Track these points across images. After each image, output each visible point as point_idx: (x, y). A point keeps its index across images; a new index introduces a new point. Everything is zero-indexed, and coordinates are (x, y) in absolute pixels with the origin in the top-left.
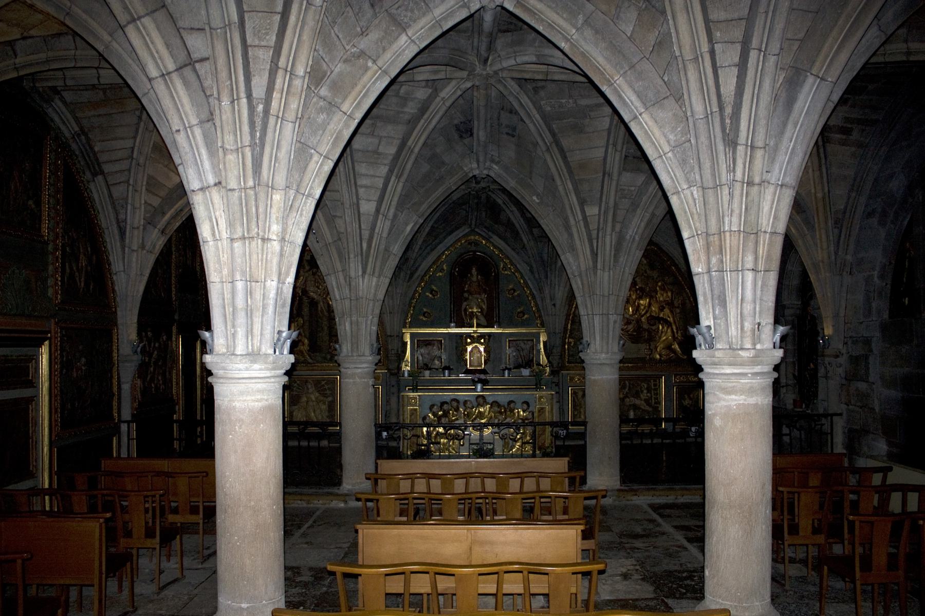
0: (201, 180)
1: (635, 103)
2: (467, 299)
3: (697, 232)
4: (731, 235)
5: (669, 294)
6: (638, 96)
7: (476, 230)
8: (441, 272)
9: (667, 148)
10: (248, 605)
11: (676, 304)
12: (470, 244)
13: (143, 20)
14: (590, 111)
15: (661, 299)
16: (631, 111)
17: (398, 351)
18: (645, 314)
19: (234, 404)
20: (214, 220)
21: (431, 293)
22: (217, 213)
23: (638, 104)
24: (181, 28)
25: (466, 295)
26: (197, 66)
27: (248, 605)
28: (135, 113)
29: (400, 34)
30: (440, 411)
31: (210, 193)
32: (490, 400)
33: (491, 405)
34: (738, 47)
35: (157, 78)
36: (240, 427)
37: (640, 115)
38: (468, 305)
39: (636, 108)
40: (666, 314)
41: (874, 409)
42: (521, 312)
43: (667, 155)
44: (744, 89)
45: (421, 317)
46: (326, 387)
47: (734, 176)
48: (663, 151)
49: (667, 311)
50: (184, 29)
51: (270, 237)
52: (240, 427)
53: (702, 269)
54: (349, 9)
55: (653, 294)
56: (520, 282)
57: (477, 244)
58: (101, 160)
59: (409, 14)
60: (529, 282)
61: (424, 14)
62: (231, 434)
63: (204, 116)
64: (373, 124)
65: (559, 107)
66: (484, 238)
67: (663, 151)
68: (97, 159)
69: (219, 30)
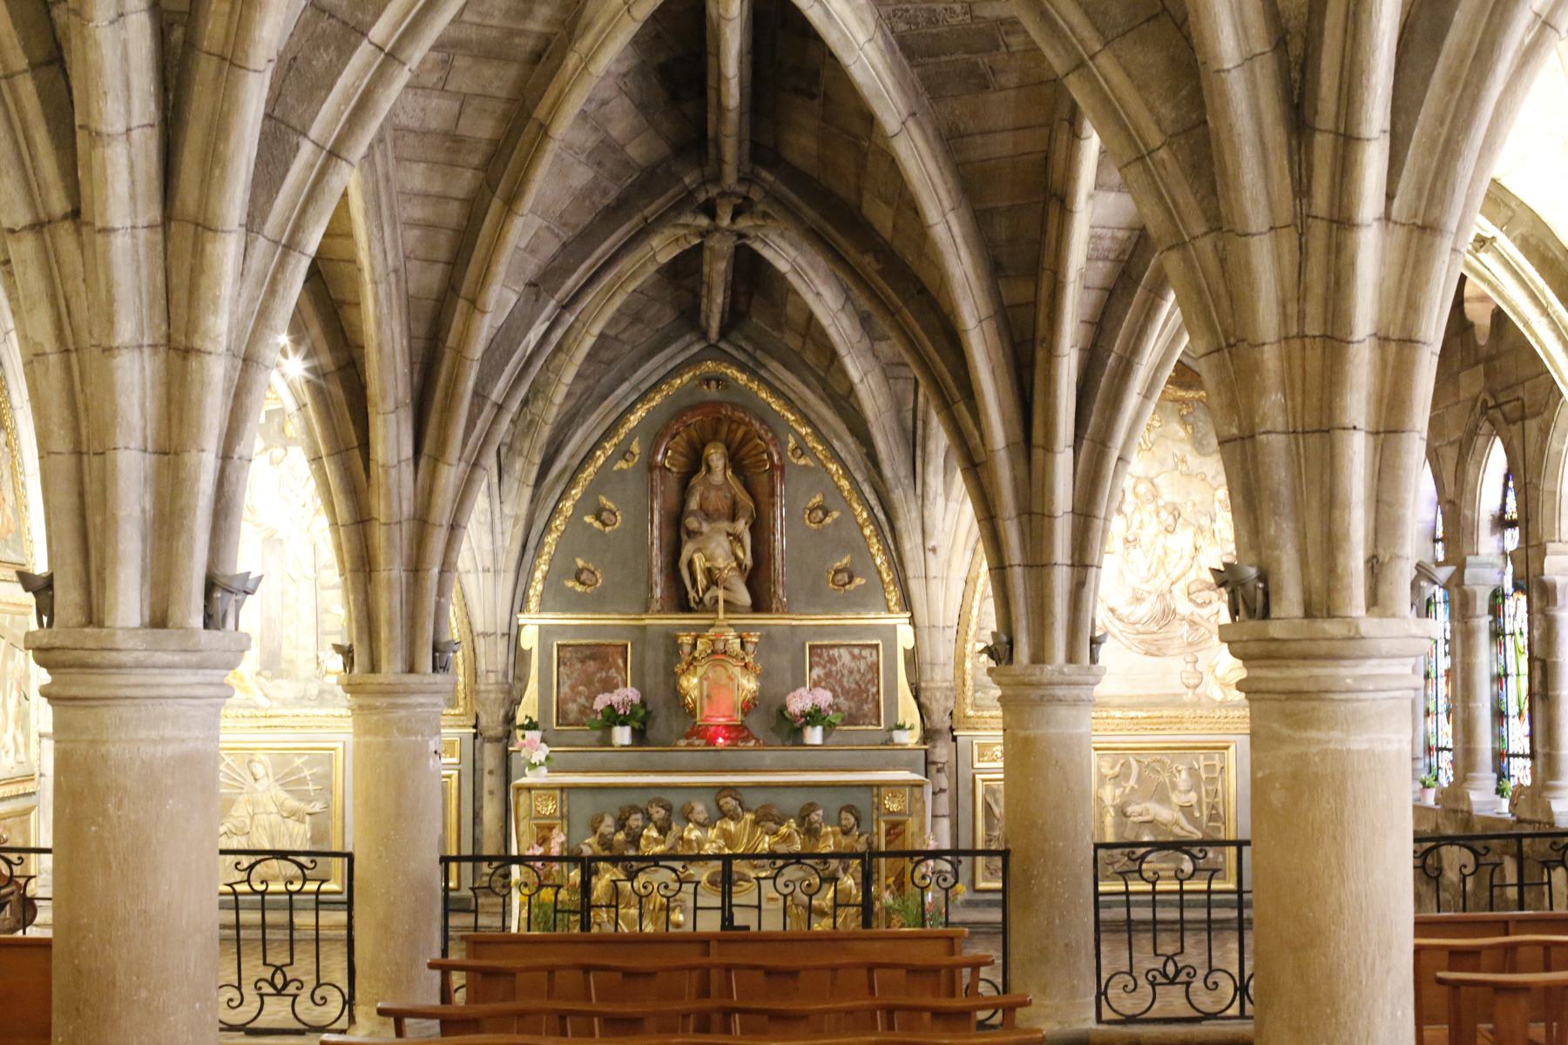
1: (1079, 30)
2: (692, 534)
3: (1227, 339)
4: (1304, 347)
6: (1087, 13)
7: (723, 345)
8: (623, 457)
9: (1155, 138)
12: (707, 381)
14: (1007, 33)
16: (1070, 49)
17: (506, 674)
19: (103, 750)
20: (62, 303)
21: (598, 517)
23: (1086, 31)
31: (52, 237)
32: (757, 799)
37: (1092, 58)
38: (699, 550)
39: (1081, 41)
43: (1154, 155)
45: (570, 584)
46: (307, 773)
47: (1310, 205)
48: (1146, 145)
53: (1240, 427)
55: (1205, 522)
56: (839, 488)
57: (721, 380)
62: (93, 823)
63: (40, 54)
64: (445, 62)
65: (929, 21)
66: (742, 368)
67: (1146, 145)
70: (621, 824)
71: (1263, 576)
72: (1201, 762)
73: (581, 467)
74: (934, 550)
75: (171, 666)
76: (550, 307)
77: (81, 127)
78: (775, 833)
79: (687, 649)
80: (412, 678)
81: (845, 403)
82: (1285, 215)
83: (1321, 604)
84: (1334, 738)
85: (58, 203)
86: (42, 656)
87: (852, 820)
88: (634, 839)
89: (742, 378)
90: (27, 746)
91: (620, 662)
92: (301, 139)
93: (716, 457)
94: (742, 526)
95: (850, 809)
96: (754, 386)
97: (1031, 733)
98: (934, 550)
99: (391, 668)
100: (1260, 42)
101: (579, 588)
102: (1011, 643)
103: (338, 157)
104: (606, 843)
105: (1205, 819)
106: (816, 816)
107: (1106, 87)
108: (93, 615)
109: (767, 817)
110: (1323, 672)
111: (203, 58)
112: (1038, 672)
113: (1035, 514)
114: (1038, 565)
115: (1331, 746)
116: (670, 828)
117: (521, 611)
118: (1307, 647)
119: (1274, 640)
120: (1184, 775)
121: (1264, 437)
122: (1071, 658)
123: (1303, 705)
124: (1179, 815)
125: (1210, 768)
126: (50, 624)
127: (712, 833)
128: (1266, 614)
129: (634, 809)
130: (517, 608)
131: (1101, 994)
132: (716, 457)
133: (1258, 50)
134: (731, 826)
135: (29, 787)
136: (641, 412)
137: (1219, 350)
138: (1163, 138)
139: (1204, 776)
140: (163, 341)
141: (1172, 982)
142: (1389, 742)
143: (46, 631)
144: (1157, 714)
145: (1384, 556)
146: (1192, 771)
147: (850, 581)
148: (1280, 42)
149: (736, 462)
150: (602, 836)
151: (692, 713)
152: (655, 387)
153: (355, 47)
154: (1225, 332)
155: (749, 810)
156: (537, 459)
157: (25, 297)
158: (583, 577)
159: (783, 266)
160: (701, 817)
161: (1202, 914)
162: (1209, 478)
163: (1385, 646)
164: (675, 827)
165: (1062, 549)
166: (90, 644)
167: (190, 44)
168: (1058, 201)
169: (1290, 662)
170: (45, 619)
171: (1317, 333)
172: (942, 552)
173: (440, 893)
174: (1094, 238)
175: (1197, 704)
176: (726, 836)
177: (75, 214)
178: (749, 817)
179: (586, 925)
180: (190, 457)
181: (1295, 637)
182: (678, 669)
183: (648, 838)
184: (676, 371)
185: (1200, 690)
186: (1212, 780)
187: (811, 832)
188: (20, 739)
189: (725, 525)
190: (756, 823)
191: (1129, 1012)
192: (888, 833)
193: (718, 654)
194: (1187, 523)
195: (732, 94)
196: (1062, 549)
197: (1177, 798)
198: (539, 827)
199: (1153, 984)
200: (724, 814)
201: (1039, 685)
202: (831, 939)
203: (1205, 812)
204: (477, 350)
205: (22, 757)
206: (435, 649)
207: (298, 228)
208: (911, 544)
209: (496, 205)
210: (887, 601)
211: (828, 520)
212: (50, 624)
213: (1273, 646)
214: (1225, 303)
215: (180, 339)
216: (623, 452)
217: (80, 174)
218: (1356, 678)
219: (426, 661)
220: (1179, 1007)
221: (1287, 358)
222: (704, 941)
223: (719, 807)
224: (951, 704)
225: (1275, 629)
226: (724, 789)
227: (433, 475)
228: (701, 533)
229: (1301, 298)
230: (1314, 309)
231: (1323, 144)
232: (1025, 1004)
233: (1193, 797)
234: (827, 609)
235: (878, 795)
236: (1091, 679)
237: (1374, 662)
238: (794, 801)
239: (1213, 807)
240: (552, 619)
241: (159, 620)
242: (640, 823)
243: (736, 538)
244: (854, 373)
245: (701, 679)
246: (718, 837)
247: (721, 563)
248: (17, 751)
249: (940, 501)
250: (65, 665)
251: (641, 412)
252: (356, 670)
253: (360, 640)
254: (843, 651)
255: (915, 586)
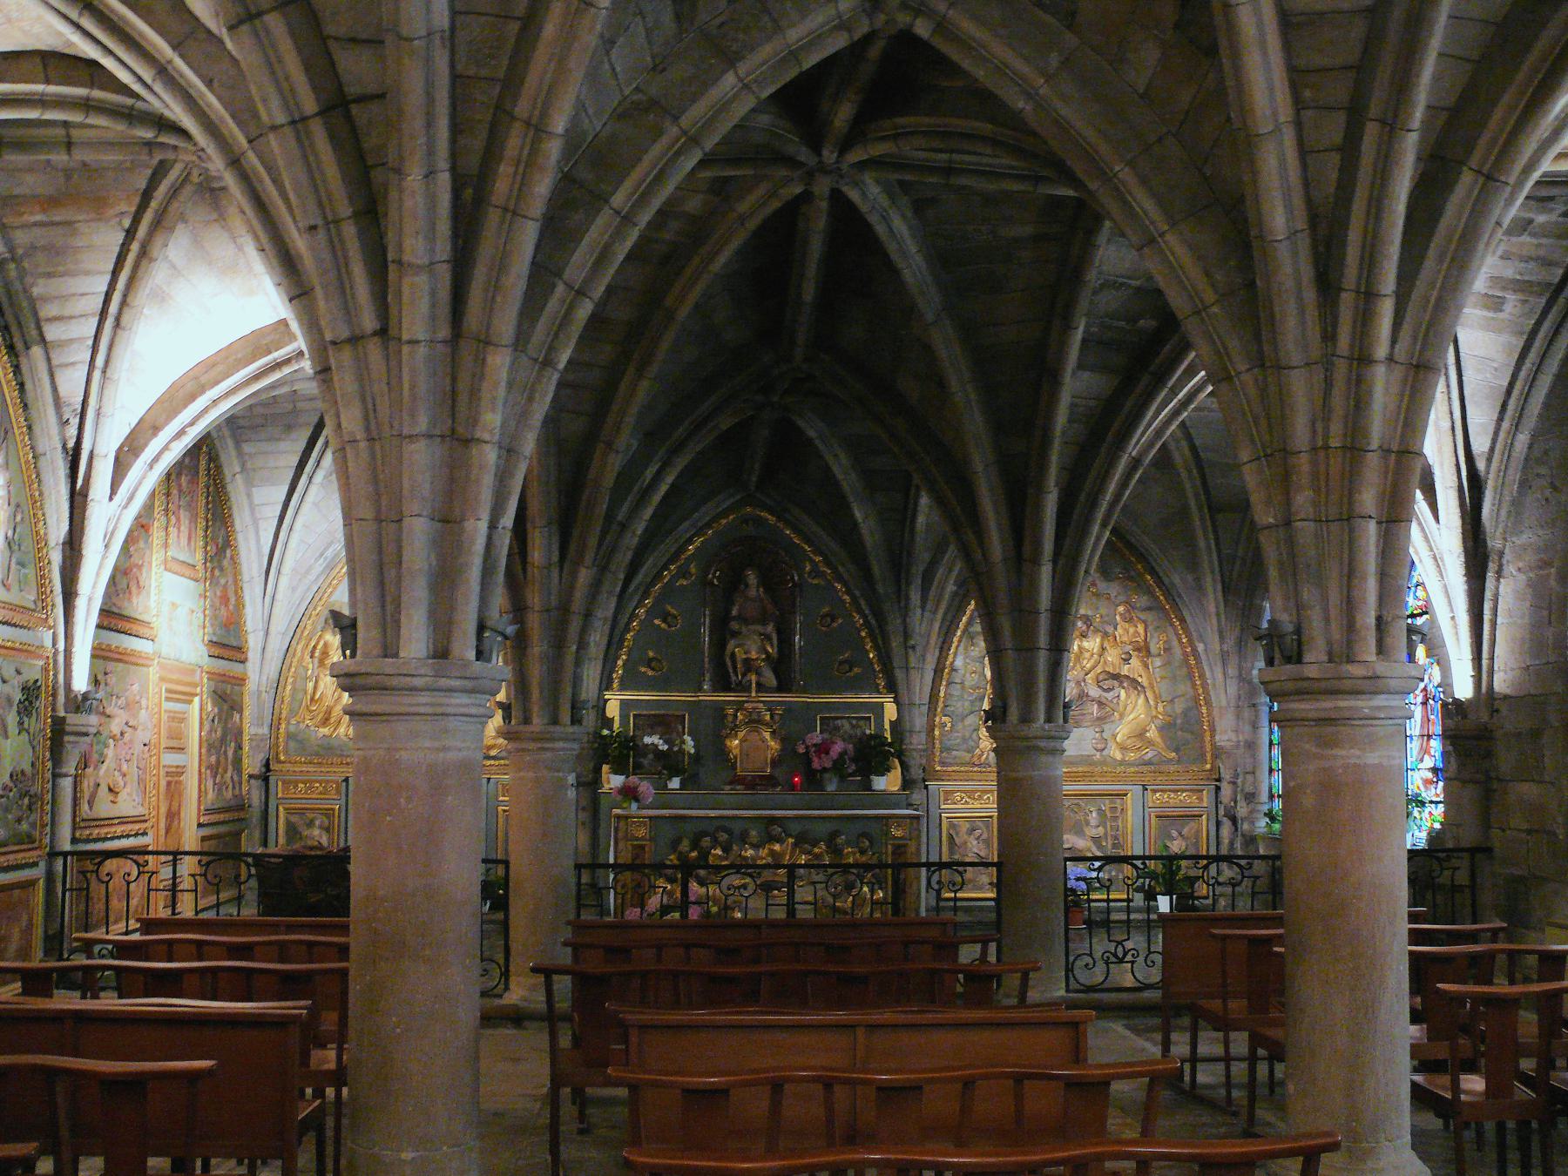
0: (350, 322)
2: (735, 634)
5: (1141, 629)
8: (684, 577)
9: (1210, 296)
10: (413, 1155)
11: (1154, 648)
12: (746, 522)
13: (267, 18)
15: (1125, 639)
18: (1094, 667)
20: (369, 399)
21: (664, 621)
22: (376, 388)
24: (329, 37)
25: (735, 625)
26: (354, 109)
27: (413, 1155)
28: (120, 223)
29: (724, 72)
30: (692, 850)
32: (795, 828)
33: (796, 838)
34: (1341, 117)
35: (283, 126)
36: (409, 799)
37: (1162, 235)
40: (1134, 667)
41: (1555, 834)
42: (845, 661)
44: (1353, 191)
49: (1135, 662)
50: (336, 39)
51: (478, 435)
52: (409, 799)
53: (1275, 517)
54: (638, 19)
55: (1110, 629)
56: (843, 602)
57: (759, 522)
58: (42, 314)
59: (741, 36)
60: (863, 603)
61: (769, 39)
68: (35, 314)
69: (416, 42)
70: (695, 845)
71: (1298, 631)
72: (1106, 805)
73: (653, 583)
74: (913, 647)
75: (451, 690)
76: (662, 452)
77: (393, 262)
78: (809, 853)
79: (730, 719)
80: (558, 728)
81: (848, 536)
82: (1315, 354)
83: (1344, 652)
84: (1346, 755)
85: (369, 322)
86: (347, 681)
87: (867, 843)
88: (705, 855)
89: (772, 519)
90: (241, 783)
91: (680, 727)
92: (556, 280)
93: (752, 577)
94: (770, 628)
95: (865, 835)
96: (780, 525)
97: (1020, 775)
98: (913, 647)
99: (538, 722)
100: (1301, 224)
101: (650, 673)
102: (1005, 708)
103: (585, 295)
104: (681, 856)
105: (1110, 847)
106: (841, 839)
107: (1171, 258)
108: (389, 649)
109: (802, 840)
110: (1364, 704)
111: (491, 209)
112: (1026, 728)
113: (1023, 610)
114: (1026, 648)
115: (1353, 761)
116: (731, 849)
117: (607, 690)
118: (1335, 684)
119: (1308, 679)
120: (1094, 814)
121: (1298, 523)
122: (1049, 720)
123: (1330, 729)
124: (1090, 844)
125: (1113, 809)
126: (353, 655)
127: (763, 852)
128: (1299, 661)
129: (704, 834)
130: (604, 686)
131: (1069, 969)
132: (752, 577)
133: (1300, 228)
134: (777, 847)
135: (242, 815)
136: (699, 541)
137: (1258, 458)
138: (1216, 297)
139: (1109, 815)
140: (449, 433)
141: (1121, 961)
142: (1394, 758)
143: (349, 661)
144: (1075, 769)
145: (1387, 617)
146: (1100, 811)
147: (850, 670)
148: (1314, 219)
149: (766, 582)
150: (681, 853)
151: (734, 767)
152: (708, 525)
153: (599, 211)
154: (1263, 445)
155: (791, 836)
156: (622, 576)
157: (342, 396)
158: (653, 664)
159: (812, 433)
160: (755, 841)
161: (1124, 917)
162: (1113, 595)
163: (1393, 683)
164: (735, 848)
165: (1043, 639)
166: (388, 670)
167: (480, 200)
168: (1052, 376)
169: (1319, 697)
170: (348, 652)
171: (1337, 445)
172: (919, 648)
173: (574, 888)
174: (1073, 406)
175: (1103, 763)
176: (772, 853)
177: (383, 332)
178: (791, 840)
179: (684, 916)
180: (469, 525)
181: (1327, 676)
182: (724, 732)
183: (715, 855)
184: (725, 514)
185: (1104, 753)
186: (1115, 818)
187: (835, 850)
188: (236, 778)
189: (759, 628)
190: (795, 845)
191: (1088, 983)
192: (893, 853)
193: (755, 722)
194: (1097, 631)
195: (809, 292)
196: (1043, 639)
197: (1092, 832)
198: (634, 847)
199: (1107, 963)
200: (773, 839)
201: (1027, 738)
202: (872, 924)
203: (1110, 842)
204: (609, 480)
205: (237, 792)
206: (573, 707)
207: (551, 349)
208: (895, 643)
209: (631, 370)
210: (878, 685)
211: (835, 625)
212: (353, 655)
213: (1305, 684)
214: (1263, 422)
215: (460, 430)
216: (682, 572)
217: (390, 298)
218: (1371, 708)
219: (566, 716)
220: (1129, 981)
221: (1314, 463)
222: (773, 924)
223: (768, 833)
224: (924, 761)
225: (1311, 671)
226: (773, 820)
227: (574, 575)
228: (740, 633)
229: (1327, 420)
230: (1336, 428)
231: (1347, 300)
232: (1037, 969)
233: (1101, 830)
234: (834, 690)
235: (886, 825)
236: (1064, 735)
237: (1382, 696)
238: (822, 829)
239: (1116, 838)
240: (628, 696)
241: (441, 652)
242: (709, 844)
243: (768, 638)
244: (858, 515)
245: (741, 741)
246: (768, 855)
247: (754, 655)
248: (234, 788)
249: (919, 611)
250: (365, 688)
251: (699, 541)
252: (513, 722)
253: (516, 698)
254: (844, 721)
255: (899, 675)
